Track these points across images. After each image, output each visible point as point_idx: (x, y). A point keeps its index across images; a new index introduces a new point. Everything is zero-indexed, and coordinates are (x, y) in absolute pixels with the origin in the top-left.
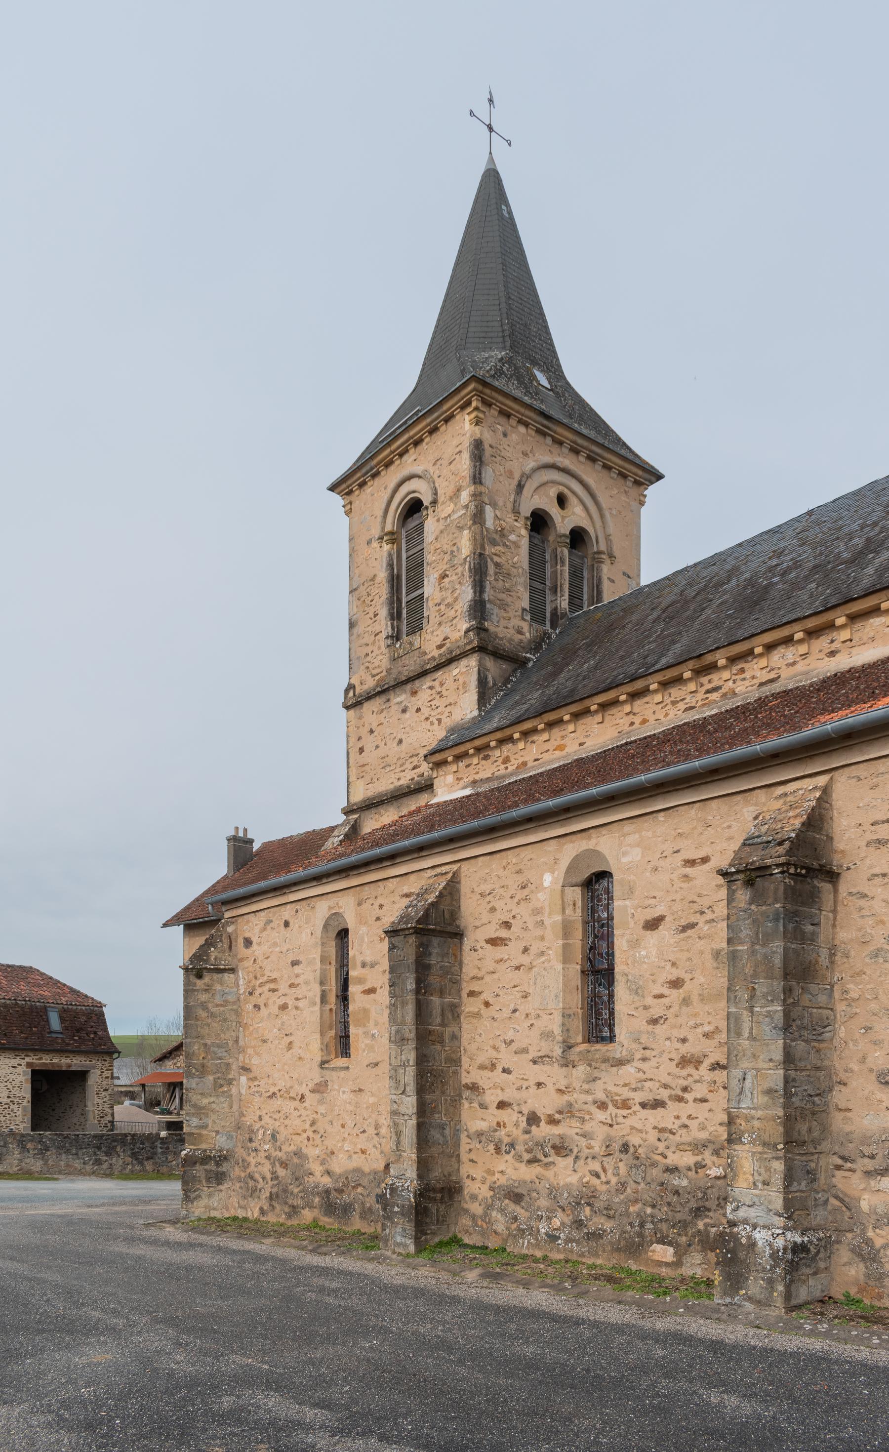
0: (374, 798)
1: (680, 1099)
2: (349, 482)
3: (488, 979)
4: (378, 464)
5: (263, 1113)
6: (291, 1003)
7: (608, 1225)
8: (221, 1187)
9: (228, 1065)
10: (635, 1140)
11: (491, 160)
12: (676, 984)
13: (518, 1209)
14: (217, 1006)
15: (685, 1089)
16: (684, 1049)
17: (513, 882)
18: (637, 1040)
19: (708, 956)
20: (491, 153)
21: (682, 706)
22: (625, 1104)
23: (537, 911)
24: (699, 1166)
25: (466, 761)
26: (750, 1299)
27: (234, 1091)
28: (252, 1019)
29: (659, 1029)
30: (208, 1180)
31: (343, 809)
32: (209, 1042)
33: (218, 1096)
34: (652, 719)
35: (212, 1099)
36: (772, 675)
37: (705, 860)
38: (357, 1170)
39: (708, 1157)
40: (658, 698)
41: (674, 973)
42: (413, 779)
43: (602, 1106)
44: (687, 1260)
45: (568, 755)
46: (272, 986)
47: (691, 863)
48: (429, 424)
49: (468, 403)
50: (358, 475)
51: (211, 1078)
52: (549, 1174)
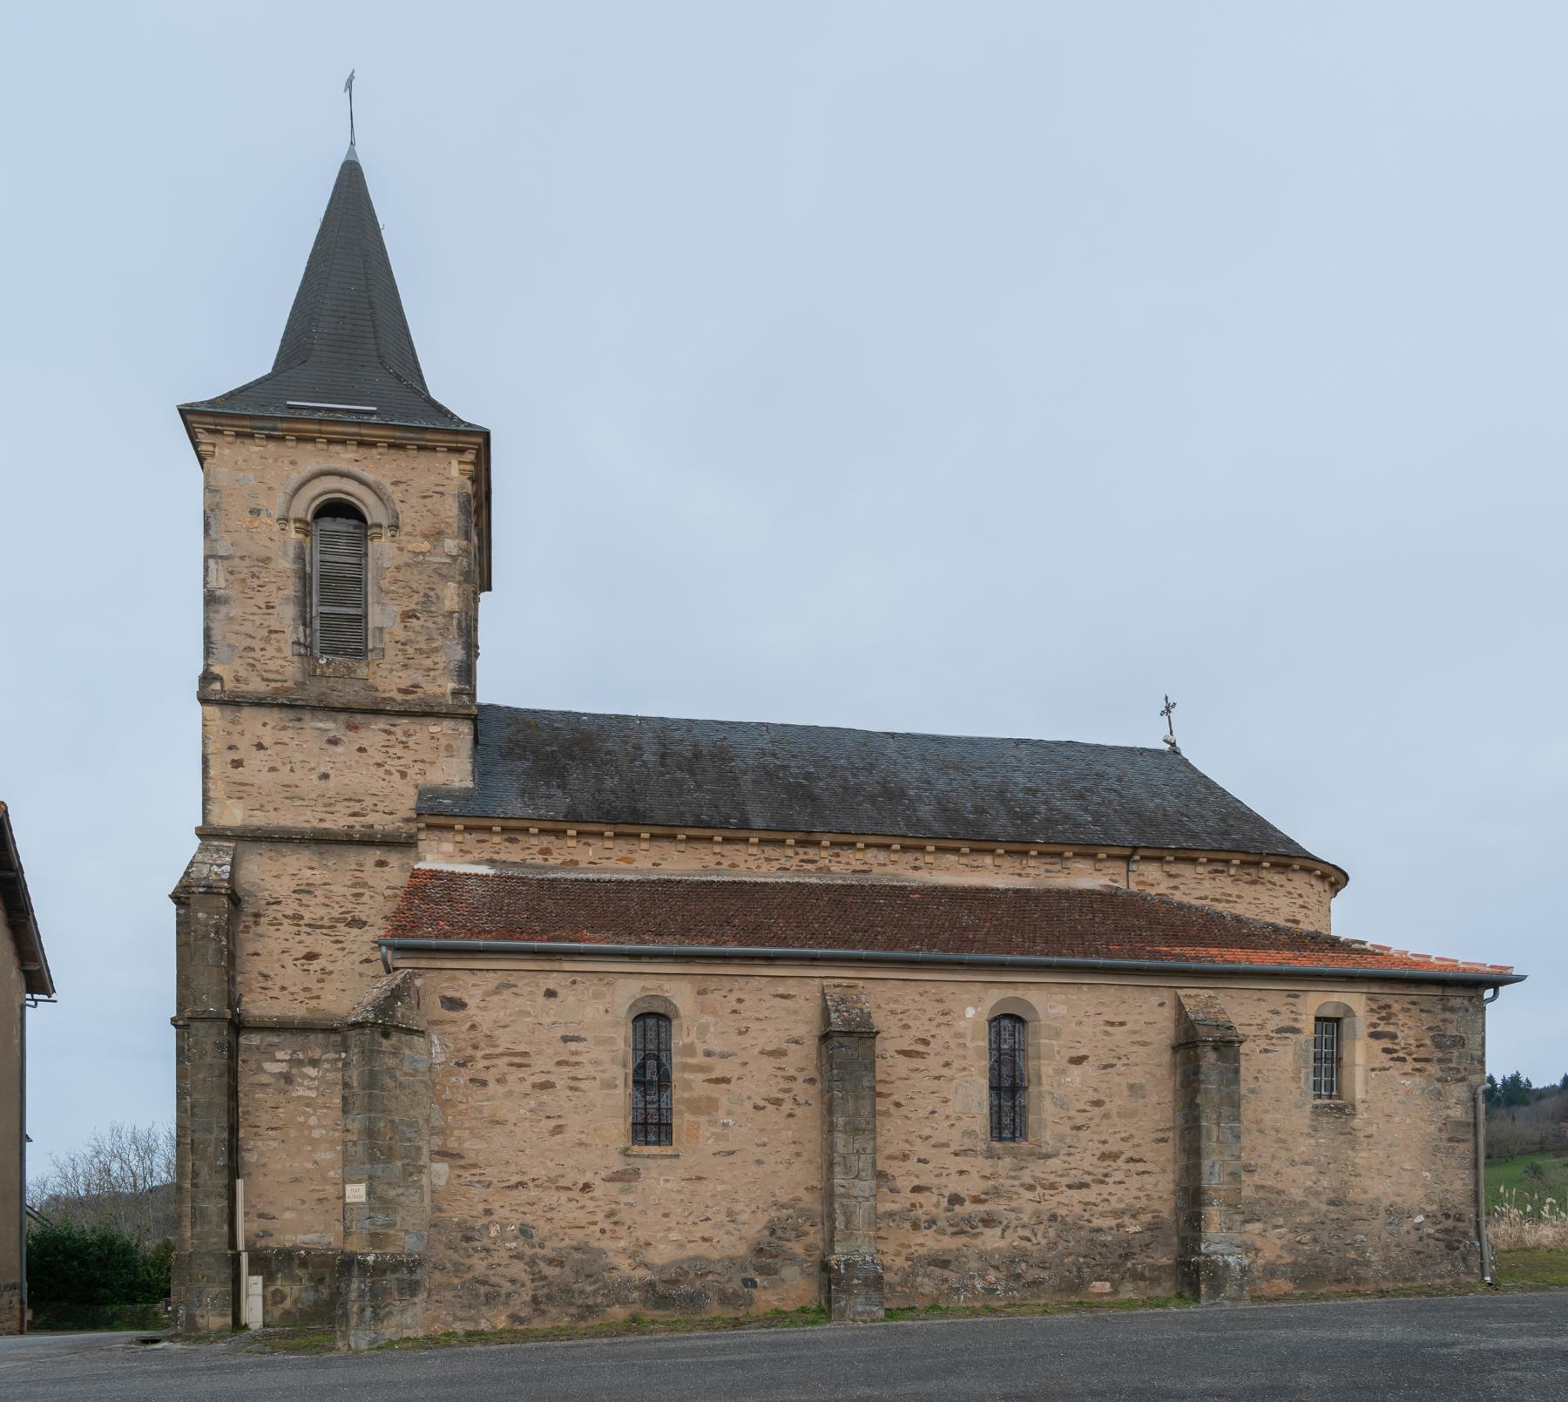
1: (1102, 1182)
2: (223, 421)
3: (899, 1083)
7: (1044, 1274)
8: (416, 1300)
9: (419, 1148)
10: (1062, 1211)
11: (352, 151)
12: (1098, 1103)
13: (946, 1273)
14: (406, 1074)
15: (1106, 1175)
16: (1105, 1148)
17: (932, 1009)
18: (1061, 1140)
19: (1124, 1087)
21: (776, 865)
22: (1053, 1186)
23: (958, 1035)
24: (1119, 1226)
26: (1227, 1298)
27: (425, 1181)
29: (1081, 1133)
30: (401, 1291)
31: (197, 829)
32: (396, 1119)
33: (407, 1187)
34: (743, 866)
35: (400, 1191)
36: (865, 867)
37: (1122, 1024)
39: (1126, 1219)
40: (753, 850)
41: (1095, 1097)
43: (1031, 1188)
44: (1122, 1289)
45: (636, 871)
47: (1112, 1024)
49: (461, 451)
51: (399, 1164)
52: (978, 1242)
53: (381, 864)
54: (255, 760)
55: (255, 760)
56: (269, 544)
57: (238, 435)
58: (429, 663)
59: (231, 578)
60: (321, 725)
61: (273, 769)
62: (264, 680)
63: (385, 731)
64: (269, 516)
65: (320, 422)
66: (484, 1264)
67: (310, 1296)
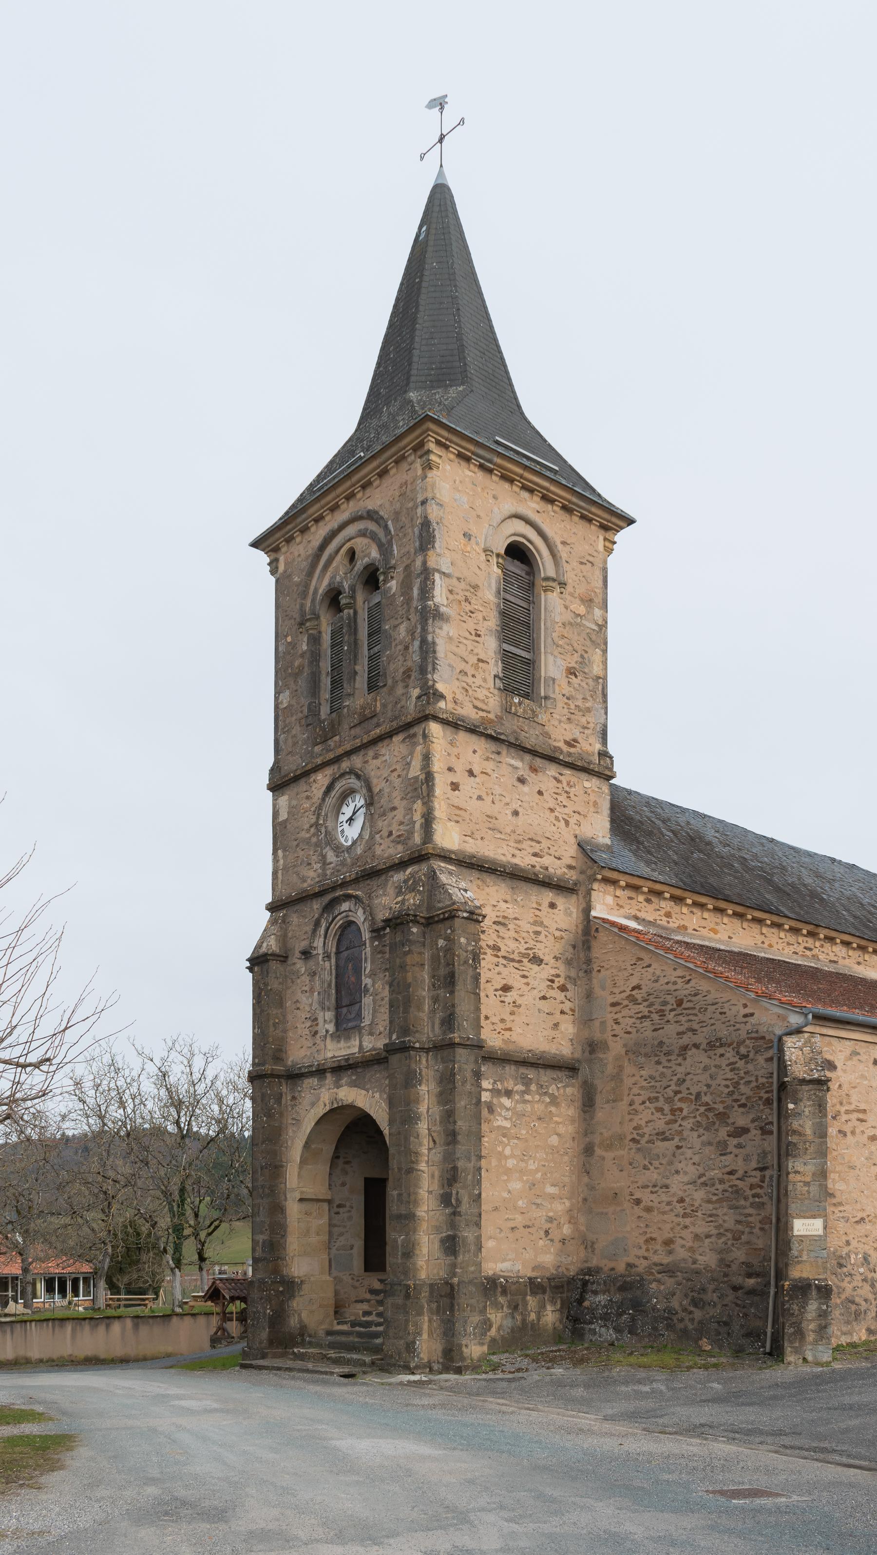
0: (487, 862)
2: (455, 439)
4: (500, 466)
5: (850, 1238)
11: (441, 174)
20: (441, 166)
25: (632, 894)
28: (837, 1145)
42: (533, 866)
46: (861, 1116)
48: (569, 501)
50: (472, 447)
53: (552, 906)
54: (468, 785)
55: (468, 785)
56: (478, 571)
57: (460, 456)
58: (583, 720)
59: (451, 597)
60: (513, 762)
61: (480, 798)
62: (476, 707)
63: (555, 778)
64: (477, 544)
65: (526, 468)
66: (851, 1286)
67: (508, 1323)
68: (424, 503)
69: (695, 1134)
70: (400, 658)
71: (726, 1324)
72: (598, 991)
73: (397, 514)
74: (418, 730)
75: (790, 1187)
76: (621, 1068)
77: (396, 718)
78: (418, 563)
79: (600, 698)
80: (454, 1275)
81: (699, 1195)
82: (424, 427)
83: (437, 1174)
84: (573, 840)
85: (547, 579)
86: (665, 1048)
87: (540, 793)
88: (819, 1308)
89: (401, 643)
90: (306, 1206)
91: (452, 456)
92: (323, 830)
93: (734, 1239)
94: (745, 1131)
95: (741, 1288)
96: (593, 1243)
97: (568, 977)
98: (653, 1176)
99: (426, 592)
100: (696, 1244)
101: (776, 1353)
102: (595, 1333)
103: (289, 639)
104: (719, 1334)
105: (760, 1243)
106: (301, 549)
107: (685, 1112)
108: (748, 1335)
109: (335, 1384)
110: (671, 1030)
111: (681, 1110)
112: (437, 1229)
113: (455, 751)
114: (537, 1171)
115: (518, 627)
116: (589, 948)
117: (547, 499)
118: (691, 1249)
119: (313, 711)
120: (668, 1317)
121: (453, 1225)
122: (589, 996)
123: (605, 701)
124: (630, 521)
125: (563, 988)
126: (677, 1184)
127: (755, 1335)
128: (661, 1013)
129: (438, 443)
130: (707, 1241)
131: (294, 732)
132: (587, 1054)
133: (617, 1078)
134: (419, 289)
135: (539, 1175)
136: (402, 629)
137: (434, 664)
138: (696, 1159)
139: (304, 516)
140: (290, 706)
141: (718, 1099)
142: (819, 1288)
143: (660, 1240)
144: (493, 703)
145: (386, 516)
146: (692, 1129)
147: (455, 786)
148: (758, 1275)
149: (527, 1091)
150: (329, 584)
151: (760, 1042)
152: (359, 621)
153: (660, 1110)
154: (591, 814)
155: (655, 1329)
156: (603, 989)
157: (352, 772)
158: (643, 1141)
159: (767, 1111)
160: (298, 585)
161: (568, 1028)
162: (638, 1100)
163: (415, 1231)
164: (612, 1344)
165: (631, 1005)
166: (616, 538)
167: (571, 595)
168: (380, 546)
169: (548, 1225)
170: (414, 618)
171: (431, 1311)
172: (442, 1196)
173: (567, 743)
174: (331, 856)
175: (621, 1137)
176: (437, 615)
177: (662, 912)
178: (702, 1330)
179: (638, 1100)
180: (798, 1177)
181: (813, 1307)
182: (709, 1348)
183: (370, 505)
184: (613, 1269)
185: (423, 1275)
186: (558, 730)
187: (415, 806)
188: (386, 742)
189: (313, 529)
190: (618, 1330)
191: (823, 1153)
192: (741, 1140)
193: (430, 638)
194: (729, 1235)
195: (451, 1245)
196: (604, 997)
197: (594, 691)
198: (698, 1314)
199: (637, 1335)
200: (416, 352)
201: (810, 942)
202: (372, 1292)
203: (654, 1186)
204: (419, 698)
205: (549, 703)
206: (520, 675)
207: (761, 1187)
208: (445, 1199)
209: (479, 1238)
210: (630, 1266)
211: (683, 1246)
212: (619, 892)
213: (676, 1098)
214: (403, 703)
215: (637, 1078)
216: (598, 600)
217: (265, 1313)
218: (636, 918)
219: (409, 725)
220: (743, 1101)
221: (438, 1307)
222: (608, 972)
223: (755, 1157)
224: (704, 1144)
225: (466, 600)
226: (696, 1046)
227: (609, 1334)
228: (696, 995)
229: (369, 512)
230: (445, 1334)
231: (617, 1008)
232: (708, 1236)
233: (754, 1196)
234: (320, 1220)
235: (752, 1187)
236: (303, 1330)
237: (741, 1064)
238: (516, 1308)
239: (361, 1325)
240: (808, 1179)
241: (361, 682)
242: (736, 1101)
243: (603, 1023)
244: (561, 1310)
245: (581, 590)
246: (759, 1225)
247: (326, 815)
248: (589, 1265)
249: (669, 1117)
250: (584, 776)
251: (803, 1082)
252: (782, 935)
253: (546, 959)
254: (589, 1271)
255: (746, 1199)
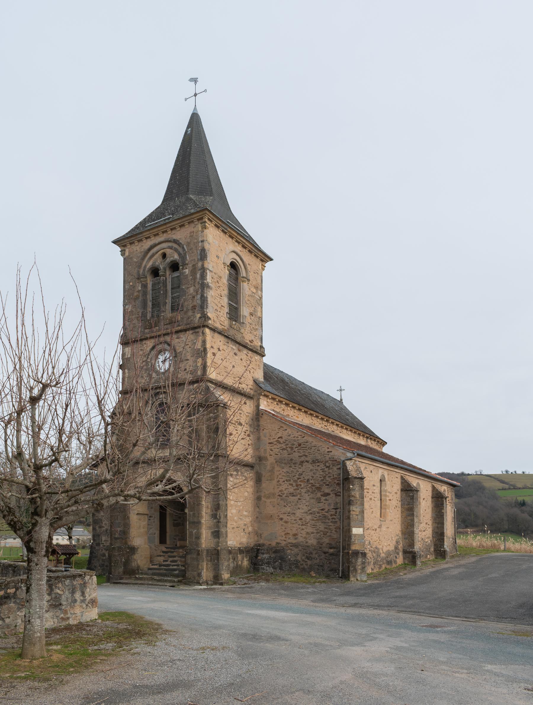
6: (373, 498)
11: (195, 108)
25: (273, 401)
38: (389, 550)
50: (220, 223)
53: (245, 403)
57: (216, 225)
58: (255, 333)
65: (238, 234)
68: (202, 241)
69: (307, 495)
70: (190, 300)
71: (321, 566)
72: (263, 437)
73: (188, 244)
74: (200, 330)
75: (351, 516)
76: (273, 468)
77: (188, 324)
78: (200, 264)
79: (260, 326)
80: (219, 546)
81: (309, 518)
82: (204, 212)
83: (210, 506)
84: (252, 379)
85: (243, 277)
86: (293, 461)
87: (241, 359)
88: (362, 561)
89: (191, 295)
90: (139, 516)
91: (213, 225)
92: (150, 364)
93: (324, 534)
94: (328, 494)
95: (327, 553)
96: (261, 534)
97: (250, 431)
98: (288, 509)
99: (203, 276)
100: (307, 536)
101: (345, 576)
102: (264, 569)
103: (131, 284)
104: (319, 570)
105: (335, 536)
106: (139, 248)
107: (302, 486)
108: (331, 570)
109: (168, 589)
110: (296, 455)
111: (301, 485)
112: (210, 528)
113: (214, 340)
114: (241, 506)
115: (234, 294)
116: (259, 421)
117: (244, 247)
118: (305, 538)
119: (144, 315)
120: (296, 564)
121: (218, 526)
122: (259, 439)
123: (262, 327)
124: (271, 260)
125: (249, 436)
126: (299, 513)
127: (334, 570)
128: (292, 448)
129: (209, 219)
130: (312, 535)
131: (134, 322)
132: (258, 461)
133: (272, 471)
134: (190, 154)
135: (241, 507)
136: (192, 290)
137: (207, 305)
138: (307, 504)
139: (141, 235)
140: (132, 311)
141: (317, 482)
142: (362, 553)
143: (291, 534)
144: (226, 323)
145: (183, 243)
146: (305, 493)
147: (214, 354)
148: (334, 548)
149: (237, 475)
150: (153, 265)
151: (335, 462)
152: (168, 282)
153: (292, 485)
154: (257, 369)
155: (290, 568)
156: (265, 437)
157: (166, 342)
158: (284, 496)
159: (338, 488)
160: (136, 262)
161: (250, 451)
162: (281, 480)
163: (201, 528)
164: (272, 574)
165: (278, 444)
166: (266, 265)
167: (251, 284)
168: (179, 254)
169: (244, 527)
170: (197, 286)
171: (207, 560)
172: (212, 515)
173: (250, 341)
174: (154, 375)
175: (274, 494)
176: (208, 287)
177: (282, 409)
178: (311, 568)
179: (281, 480)
180: (354, 513)
181: (360, 560)
182: (314, 575)
183: (174, 237)
184: (270, 545)
185: (204, 546)
186: (247, 337)
187: (198, 360)
188: (183, 333)
189: (144, 241)
190: (274, 568)
191: (362, 504)
192: (327, 498)
193: (205, 295)
194: (322, 533)
195: (217, 534)
196: (266, 440)
197: (258, 322)
198: (309, 562)
199: (283, 570)
200: (191, 179)
201: (326, 424)
202: (163, 552)
203: (289, 513)
204: (200, 318)
205: (244, 325)
206: (234, 313)
207: (335, 515)
208: (214, 516)
209: (227, 532)
210: (278, 543)
211: (302, 536)
212: (268, 400)
213: (299, 481)
214: (192, 318)
215: (281, 472)
216: (260, 287)
217: (121, 561)
218: (274, 410)
219: (195, 328)
220: (328, 483)
221: (211, 559)
222: (267, 431)
223: (333, 505)
224: (310, 498)
225: (217, 282)
226: (307, 462)
227: (271, 570)
228: (307, 442)
229: (174, 240)
230: (214, 569)
231: (272, 445)
232: (312, 533)
233: (332, 519)
234: (144, 522)
235: (331, 515)
236: (138, 567)
237: (326, 469)
238: (234, 559)
239: (164, 565)
240: (358, 513)
241: (168, 307)
242: (325, 483)
243: (265, 450)
244: (249, 560)
245: (254, 283)
246: (334, 529)
247: (152, 358)
248: (259, 543)
249: (295, 488)
250: (255, 354)
251: (356, 478)
252: (318, 420)
253: (243, 424)
254: (259, 545)
255: (329, 519)
